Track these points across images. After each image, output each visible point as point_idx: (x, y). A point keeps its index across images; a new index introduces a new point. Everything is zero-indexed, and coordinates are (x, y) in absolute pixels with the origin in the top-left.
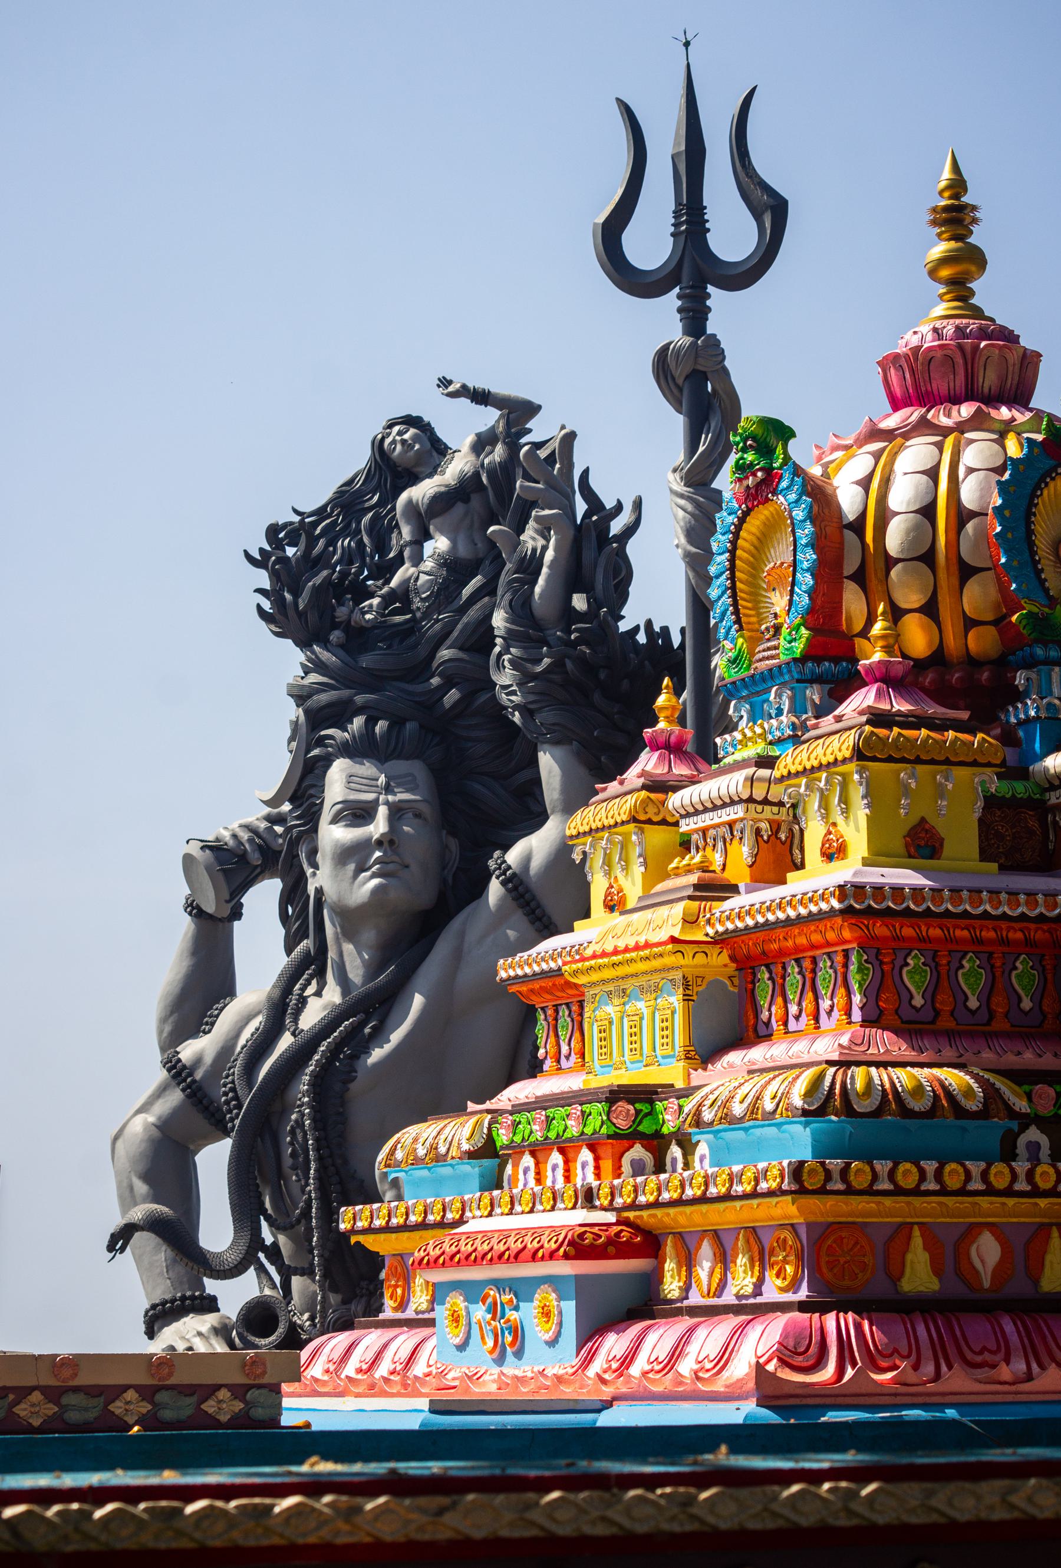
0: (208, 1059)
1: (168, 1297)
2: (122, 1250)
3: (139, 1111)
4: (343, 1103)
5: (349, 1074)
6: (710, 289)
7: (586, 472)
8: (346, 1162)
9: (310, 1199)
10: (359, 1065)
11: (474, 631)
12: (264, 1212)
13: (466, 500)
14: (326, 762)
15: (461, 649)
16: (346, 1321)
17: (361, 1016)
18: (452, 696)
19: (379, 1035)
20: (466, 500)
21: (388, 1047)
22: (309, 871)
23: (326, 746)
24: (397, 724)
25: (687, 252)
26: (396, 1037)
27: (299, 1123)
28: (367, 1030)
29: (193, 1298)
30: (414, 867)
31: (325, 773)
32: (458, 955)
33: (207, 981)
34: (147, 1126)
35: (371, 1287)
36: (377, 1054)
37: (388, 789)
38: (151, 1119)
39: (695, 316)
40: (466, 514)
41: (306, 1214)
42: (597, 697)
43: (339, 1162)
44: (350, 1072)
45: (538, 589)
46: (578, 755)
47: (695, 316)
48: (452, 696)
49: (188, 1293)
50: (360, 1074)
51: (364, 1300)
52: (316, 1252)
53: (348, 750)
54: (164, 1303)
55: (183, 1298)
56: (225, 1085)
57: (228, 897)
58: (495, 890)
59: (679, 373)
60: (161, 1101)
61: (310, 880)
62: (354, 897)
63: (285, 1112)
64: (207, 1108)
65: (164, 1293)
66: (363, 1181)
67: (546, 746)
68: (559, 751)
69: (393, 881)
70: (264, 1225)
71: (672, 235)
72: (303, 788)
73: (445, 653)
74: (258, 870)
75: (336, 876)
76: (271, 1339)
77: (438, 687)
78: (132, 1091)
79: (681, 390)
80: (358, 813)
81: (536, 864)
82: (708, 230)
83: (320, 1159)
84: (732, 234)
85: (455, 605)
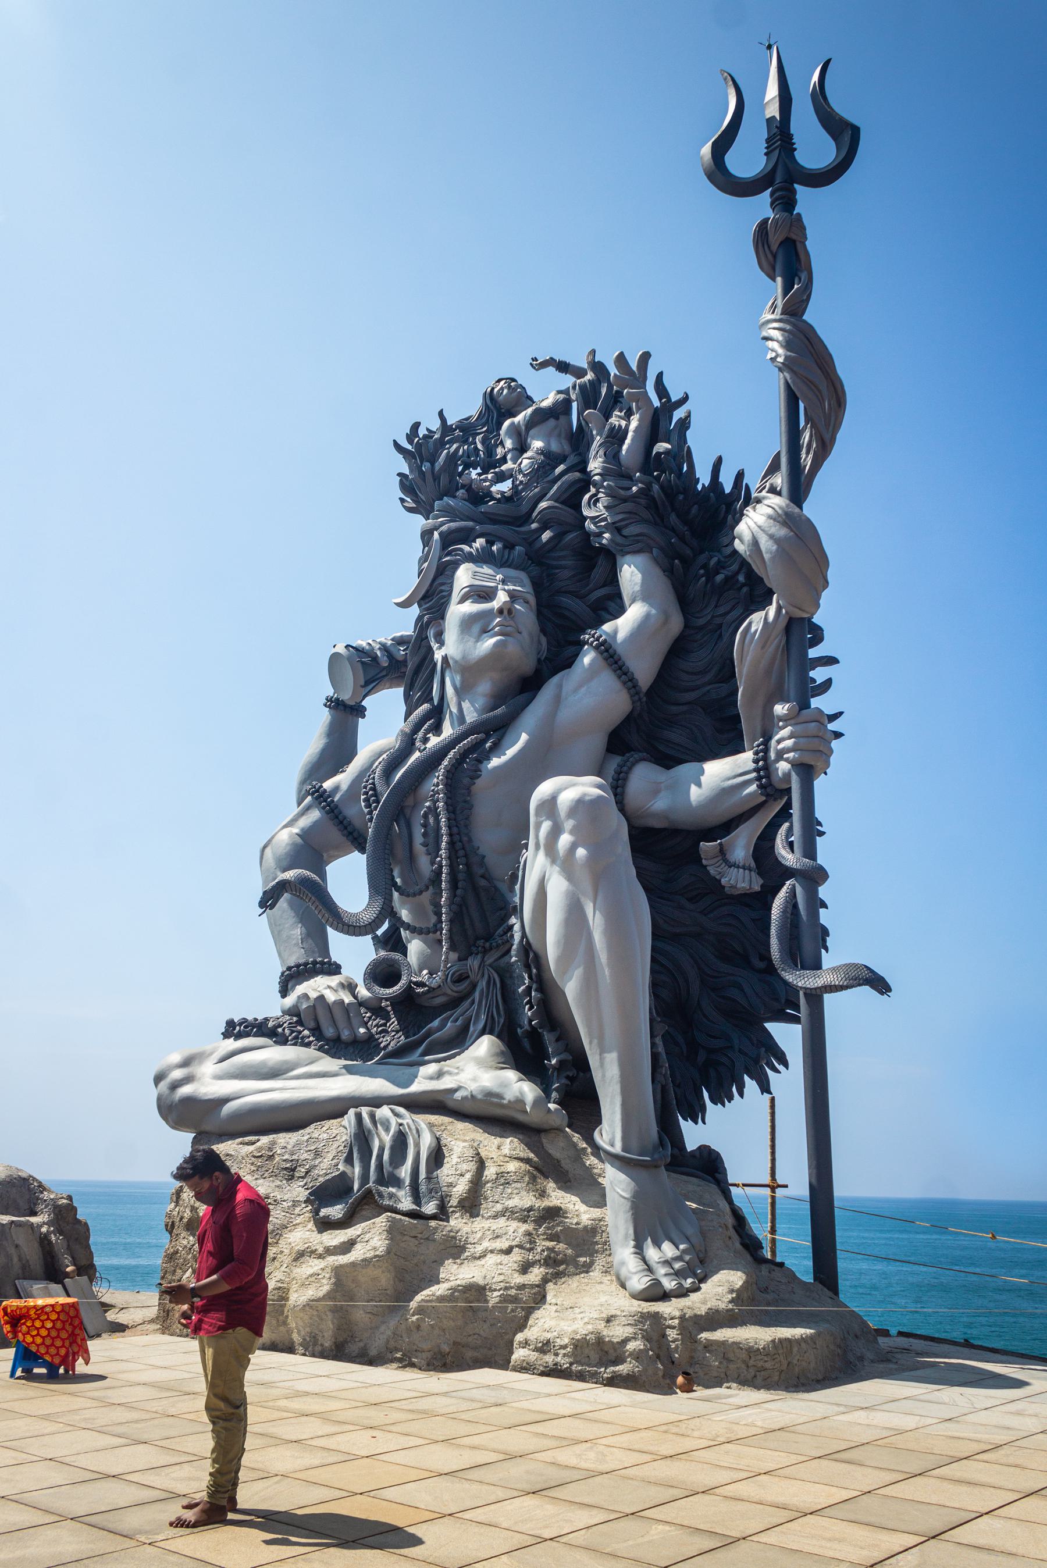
0: (344, 787)
1: (302, 961)
2: (272, 907)
3: (285, 826)
4: (469, 793)
5: (476, 774)
6: (796, 186)
7: (660, 376)
8: (470, 840)
9: (441, 866)
10: (482, 767)
11: (566, 490)
12: (395, 884)
13: (557, 419)
14: (456, 565)
15: (555, 501)
16: (461, 975)
17: (481, 736)
18: (546, 536)
19: (497, 748)
20: (557, 419)
21: (504, 759)
22: (435, 646)
23: (456, 555)
24: (509, 546)
25: (780, 160)
26: (510, 753)
27: (433, 810)
28: (488, 745)
29: (322, 963)
30: (525, 634)
31: (454, 573)
32: (558, 700)
33: (339, 748)
34: (291, 836)
35: (487, 945)
36: (495, 762)
37: (504, 582)
38: (295, 830)
39: (785, 202)
40: (556, 427)
41: (436, 879)
42: (673, 518)
43: (465, 839)
44: (476, 771)
45: (625, 447)
46: (656, 561)
47: (785, 202)
48: (546, 536)
49: (319, 959)
50: (484, 773)
51: (479, 956)
52: (444, 910)
53: (469, 558)
54: (298, 966)
55: (315, 963)
56: (365, 787)
57: (363, 683)
58: (588, 658)
59: (775, 240)
60: (304, 817)
61: (436, 652)
62: (477, 652)
63: (417, 805)
64: (341, 822)
65: (298, 958)
66: (484, 857)
67: (628, 558)
68: (641, 559)
69: (510, 639)
70: (396, 895)
71: (766, 154)
72: (432, 598)
73: (543, 505)
74: (384, 673)
75: (463, 638)
76: (391, 990)
77: (536, 530)
78: (282, 818)
79: (775, 256)
80: (483, 594)
81: (621, 636)
82: (795, 149)
83: (450, 835)
84: (814, 148)
85: (551, 477)
